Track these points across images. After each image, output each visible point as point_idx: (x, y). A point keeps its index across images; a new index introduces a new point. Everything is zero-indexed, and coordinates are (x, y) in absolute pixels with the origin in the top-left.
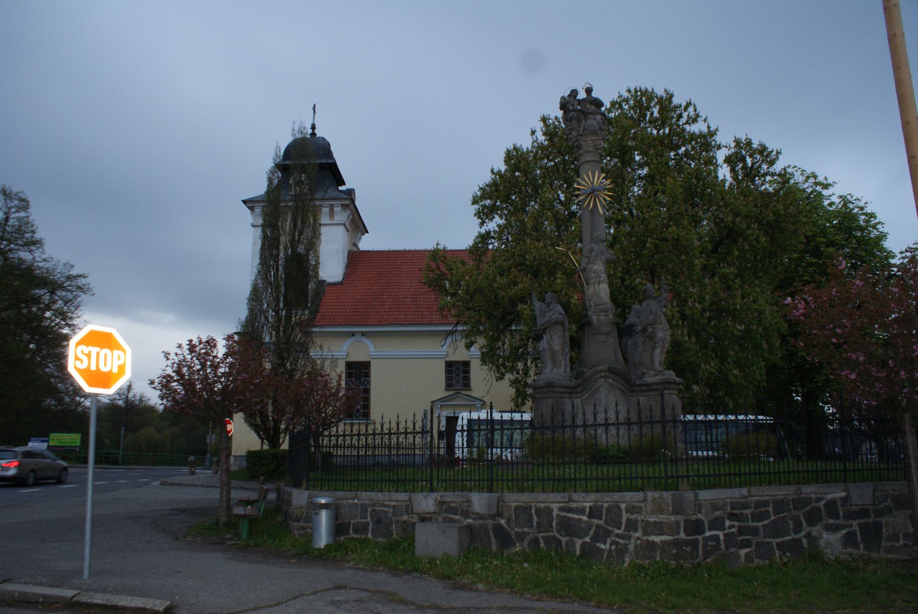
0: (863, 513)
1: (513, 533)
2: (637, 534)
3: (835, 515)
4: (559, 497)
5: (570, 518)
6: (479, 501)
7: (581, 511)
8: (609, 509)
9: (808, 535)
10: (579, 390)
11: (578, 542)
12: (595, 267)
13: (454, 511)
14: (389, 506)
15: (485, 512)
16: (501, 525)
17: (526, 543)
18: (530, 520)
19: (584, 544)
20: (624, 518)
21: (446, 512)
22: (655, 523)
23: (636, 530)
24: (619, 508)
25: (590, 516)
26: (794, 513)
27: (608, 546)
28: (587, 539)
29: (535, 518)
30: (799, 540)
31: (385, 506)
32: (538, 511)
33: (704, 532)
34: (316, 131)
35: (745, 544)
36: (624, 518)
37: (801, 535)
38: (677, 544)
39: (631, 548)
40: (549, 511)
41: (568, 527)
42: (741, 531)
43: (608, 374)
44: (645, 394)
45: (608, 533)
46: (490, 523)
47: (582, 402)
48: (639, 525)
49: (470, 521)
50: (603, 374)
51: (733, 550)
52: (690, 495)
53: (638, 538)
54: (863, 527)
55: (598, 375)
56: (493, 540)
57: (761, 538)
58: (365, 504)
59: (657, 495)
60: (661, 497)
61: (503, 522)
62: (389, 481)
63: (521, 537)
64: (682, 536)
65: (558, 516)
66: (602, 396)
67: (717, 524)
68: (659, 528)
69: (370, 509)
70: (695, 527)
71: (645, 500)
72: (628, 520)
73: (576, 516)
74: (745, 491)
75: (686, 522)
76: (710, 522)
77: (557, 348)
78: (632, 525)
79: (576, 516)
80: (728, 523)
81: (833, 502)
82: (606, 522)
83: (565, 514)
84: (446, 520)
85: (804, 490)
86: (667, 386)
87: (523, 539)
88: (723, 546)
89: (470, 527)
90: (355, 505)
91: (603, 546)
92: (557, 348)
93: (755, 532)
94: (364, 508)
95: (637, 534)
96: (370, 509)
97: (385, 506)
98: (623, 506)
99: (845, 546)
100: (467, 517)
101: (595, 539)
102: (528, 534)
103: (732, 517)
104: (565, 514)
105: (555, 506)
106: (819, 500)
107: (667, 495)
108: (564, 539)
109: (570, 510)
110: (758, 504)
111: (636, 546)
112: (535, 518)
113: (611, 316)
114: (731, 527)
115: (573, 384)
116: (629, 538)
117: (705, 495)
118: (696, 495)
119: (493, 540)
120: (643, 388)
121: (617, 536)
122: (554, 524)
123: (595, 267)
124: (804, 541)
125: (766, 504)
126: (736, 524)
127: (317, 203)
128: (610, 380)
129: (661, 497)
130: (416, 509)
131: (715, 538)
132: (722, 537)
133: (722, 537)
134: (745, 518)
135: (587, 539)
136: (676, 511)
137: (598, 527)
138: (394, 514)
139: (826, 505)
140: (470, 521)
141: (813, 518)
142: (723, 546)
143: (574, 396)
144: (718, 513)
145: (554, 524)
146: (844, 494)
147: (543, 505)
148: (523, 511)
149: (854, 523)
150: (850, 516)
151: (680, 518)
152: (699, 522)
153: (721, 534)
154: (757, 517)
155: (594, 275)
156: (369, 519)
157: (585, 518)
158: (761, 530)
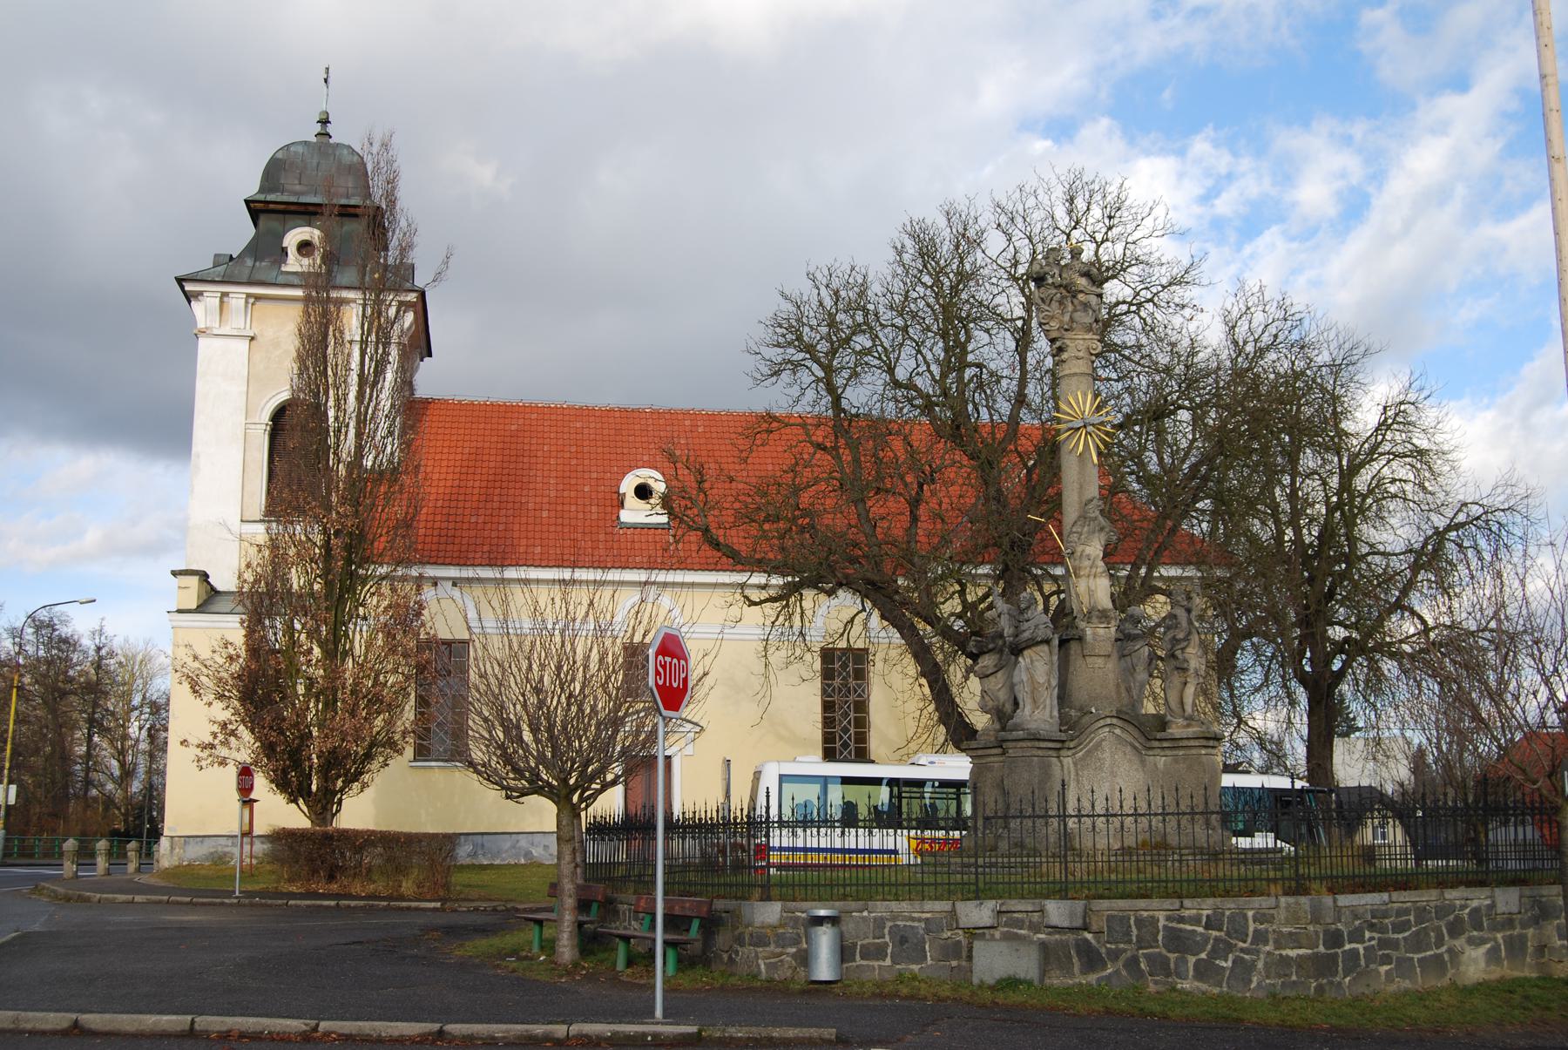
0: (1509, 922)
1: (1103, 951)
2: (1267, 948)
3: (1479, 927)
4: (1167, 903)
5: (1181, 930)
6: (1057, 912)
7: (1196, 920)
8: (1232, 919)
9: (1450, 951)
10: (1072, 745)
11: (1192, 960)
12: (1088, 550)
13: (1019, 924)
14: (919, 920)
15: (1066, 924)
16: (1086, 940)
17: (1120, 963)
18: (1128, 933)
19: (1198, 961)
20: (1251, 929)
21: (1006, 925)
22: (1290, 934)
23: (1266, 943)
24: (1245, 917)
25: (1207, 927)
26: (1436, 923)
27: (1230, 964)
28: (1203, 956)
29: (1135, 931)
30: (1441, 955)
31: (913, 919)
32: (1140, 923)
33: (1341, 945)
34: (330, 129)
35: (1386, 960)
36: (1251, 929)
37: (1444, 949)
38: (1316, 957)
39: (1260, 965)
40: (1155, 921)
41: (1178, 941)
42: (1383, 944)
43: (1115, 721)
44: (1168, 752)
45: (1230, 948)
46: (1070, 938)
47: (1075, 764)
48: (1271, 937)
49: (1042, 936)
50: (1108, 721)
51: (1372, 966)
52: (1328, 900)
53: (1269, 953)
54: (1509, 941)
55: (1102, 722)
56: (1075, 960)
57: (1402, 953)
58: (882, 918)
59: (1291, 900)
60: (1297, 903)
61: (1089, 936)
62: (793, 885)
63: (1114, 955)
64: (1321, 949)
65: (1165, 927)
66: (1107, 755)
67: (1356, 936)
68: (1295, 940)
69: (889, 924)
70: (1334, 939)
71: (1277, 907)
72: (1256, 931)
73: (1189, 927)
74: (1385, 896)
75: (1326, 932)
76: (1350, 933)
77: (1041, 678)
78: (1260, 937)
79: (1189, 927)
80: (1367, 935)
81: (1476, 911)
82: (1228, 934)
83: (1174, 925)
84: (1007, 937)
85: (1447, 896)
86: (1204, 743)
87: (1117, 958)
88: (1363, 962)
89: (1043, 945)
90: (864, 918)
91: (1224, 964)
92: (1041, 678)
93: (1394, 945)
94: (879, 923)
95: (1267, 948)
96: (889, 924)
97: (913, 919)
98: (1250, 914)
99: (1488, 963)
100: (1039, 932)
101: (1214, 954)
102: (1125, 951)
103: (1372, 927)
104: (1174, 925)
105: (1161, 916)
106: (1463, 907)
107: (1304, 900)
108: (1172, 956)
109: (1181, 920)
110: (1399, 913)
111: (1266, 963)
112: (1135, 931)
113: (1113, 630)
114: (1371, 939)
115: (1063, 736)
116: (1258, 952)
117: (1344, 900)
118: (1335, 901)
119: (1075, 960)
120: (1165, 744)
121: (1242, 950)
122: (1160, 938)
123: (1088, 550)
124: (1446, 957)
125: (1407, 912)
126: (1376, 935)
127: (334, 294)
128: (1117, 731)
129: (1297, 903)
130: (964, 922)
131: (1355, 952)
132: (1362, 952)
133: (1362, 952)
134: (1383, 930)
135: (1203, 956)
136: (1316, 920)
137: (1216, 939)
138: (928, 931)
139: (1470, 914)
140: (1042, 936)
141: (1456, 929)
142: (1363, 962)
143: (1064, 753)
144: (1357, 923)
145: (1160, 938)
146: (1488, 902)
147: (1145, 914)
148: (1118, 925)
149: (1499, 936)
150: (1495, 928)
151: (1319, 928)
152: (1338, 933)
153: (1360, 947)
154: (1399, 928)
155: (1087, 563)
156: (887, 939)
157: (1200, 930)
158: (1467, 926)
